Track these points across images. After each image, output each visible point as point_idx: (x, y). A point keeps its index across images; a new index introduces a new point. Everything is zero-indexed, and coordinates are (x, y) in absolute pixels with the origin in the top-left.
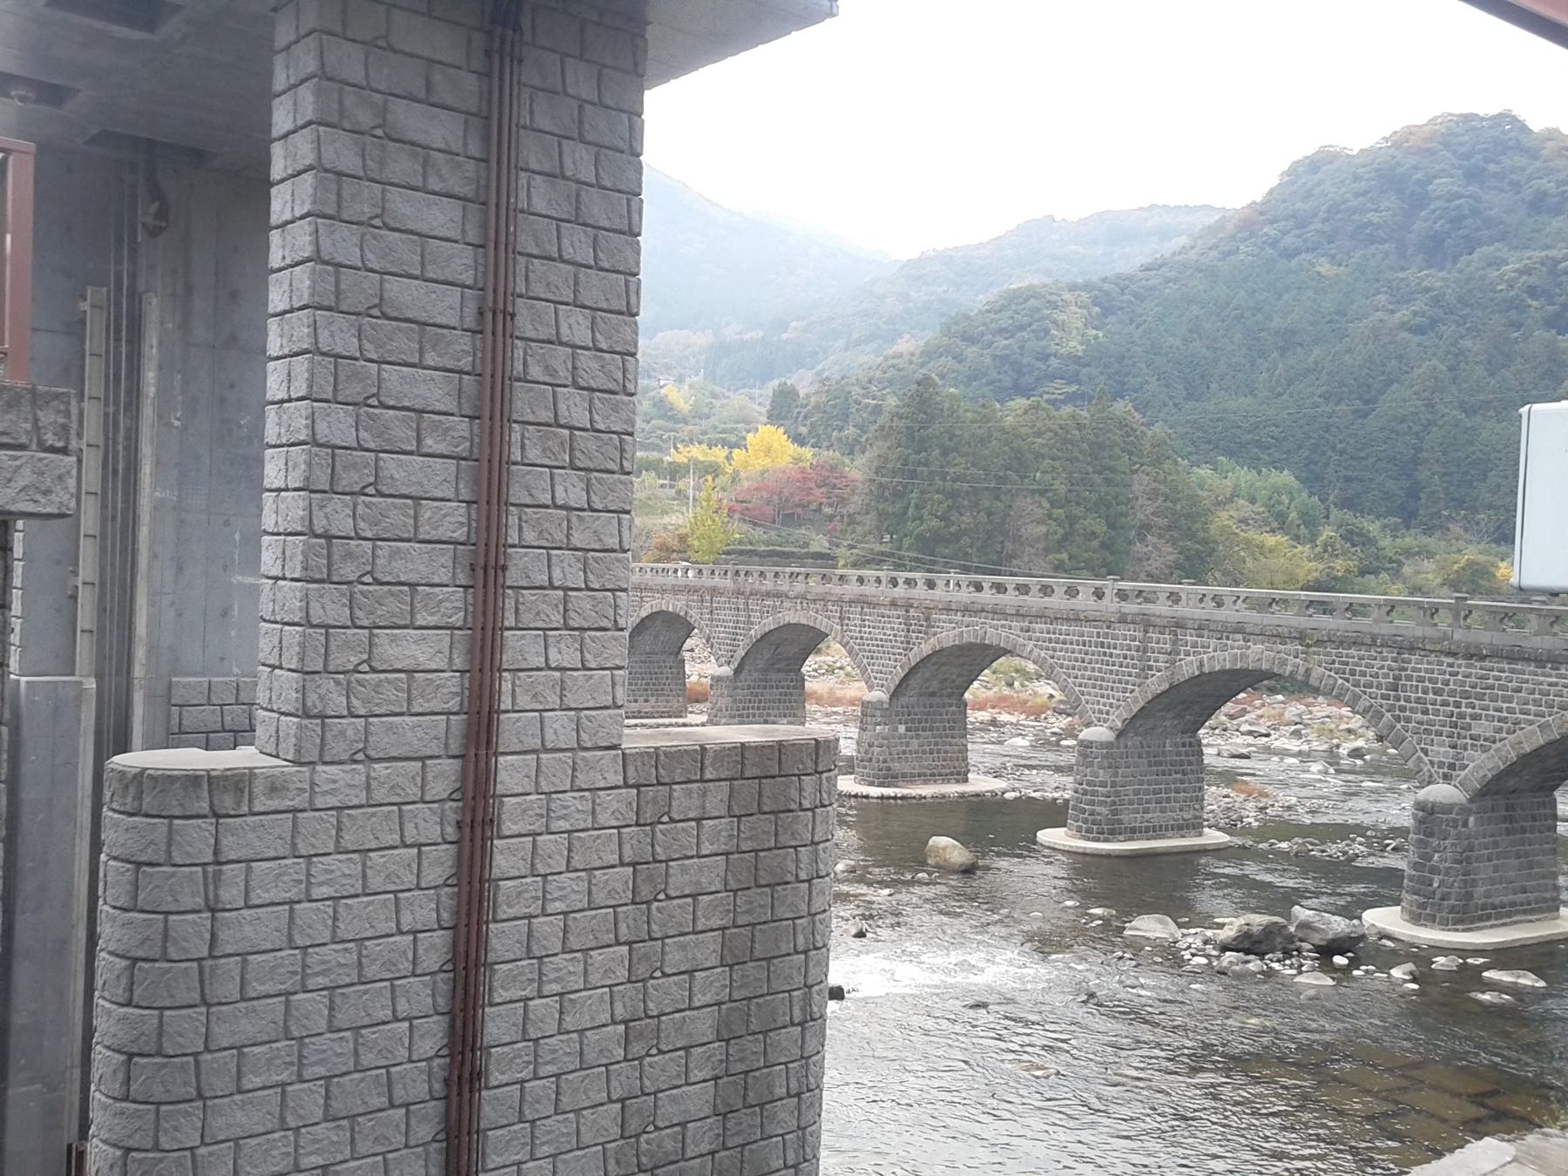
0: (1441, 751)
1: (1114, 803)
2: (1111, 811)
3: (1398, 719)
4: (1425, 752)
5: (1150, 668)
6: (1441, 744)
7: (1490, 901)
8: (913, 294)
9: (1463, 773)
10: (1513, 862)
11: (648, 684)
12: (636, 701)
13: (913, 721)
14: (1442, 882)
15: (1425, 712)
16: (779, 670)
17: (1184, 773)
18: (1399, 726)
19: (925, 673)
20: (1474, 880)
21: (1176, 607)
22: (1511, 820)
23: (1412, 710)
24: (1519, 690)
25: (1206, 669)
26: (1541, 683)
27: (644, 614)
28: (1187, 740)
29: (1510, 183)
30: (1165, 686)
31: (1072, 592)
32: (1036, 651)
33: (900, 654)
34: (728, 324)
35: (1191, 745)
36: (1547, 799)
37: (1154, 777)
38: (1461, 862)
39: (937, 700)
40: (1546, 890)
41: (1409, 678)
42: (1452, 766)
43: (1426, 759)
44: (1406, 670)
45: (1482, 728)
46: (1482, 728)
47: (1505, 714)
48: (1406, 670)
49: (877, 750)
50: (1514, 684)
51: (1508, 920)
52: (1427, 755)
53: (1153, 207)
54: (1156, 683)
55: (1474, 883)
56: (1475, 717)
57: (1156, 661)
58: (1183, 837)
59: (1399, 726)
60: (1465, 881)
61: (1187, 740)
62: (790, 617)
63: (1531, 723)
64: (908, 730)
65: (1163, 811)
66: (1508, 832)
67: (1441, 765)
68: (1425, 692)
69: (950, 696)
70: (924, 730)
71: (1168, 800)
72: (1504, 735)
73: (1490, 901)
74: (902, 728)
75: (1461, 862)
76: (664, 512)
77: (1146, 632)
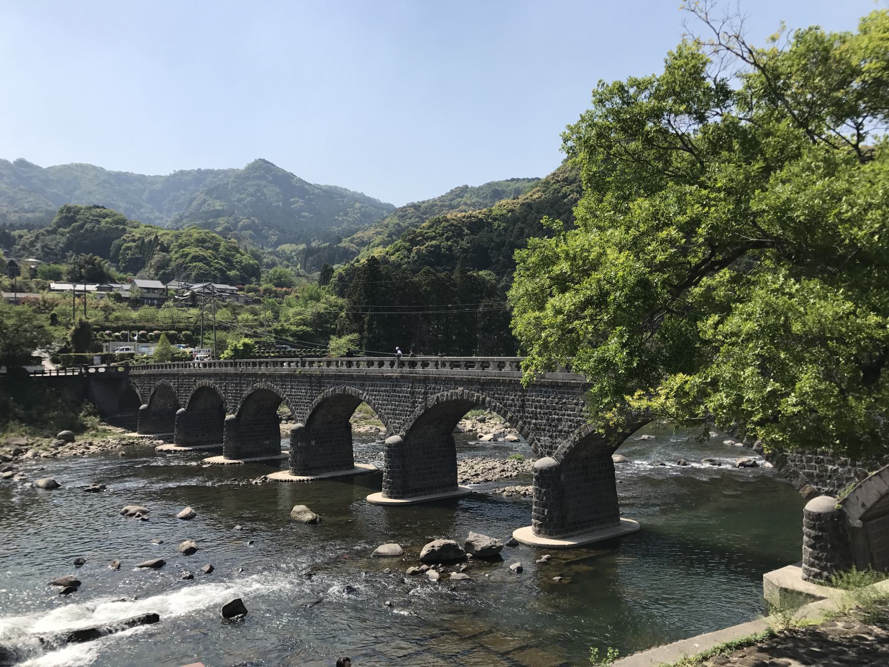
4: (539, 441)
8: (402, 224)
12: (197, 436)
21: (426, 369)
30: (423, 411)
31: (501, 365)
33: (309, 402)
34: (314, 240)
41: (528, 400)
42: (551, 447)
46: (564, 426)
51: (589, 529)
53: (513, 180)
54: (419, 411)
57: (419, 398)
58: (445, 492)
64: (316, 443)
67: (546, 447)
68: (536, 408)
74: (313, 443)
76: (261, 337)
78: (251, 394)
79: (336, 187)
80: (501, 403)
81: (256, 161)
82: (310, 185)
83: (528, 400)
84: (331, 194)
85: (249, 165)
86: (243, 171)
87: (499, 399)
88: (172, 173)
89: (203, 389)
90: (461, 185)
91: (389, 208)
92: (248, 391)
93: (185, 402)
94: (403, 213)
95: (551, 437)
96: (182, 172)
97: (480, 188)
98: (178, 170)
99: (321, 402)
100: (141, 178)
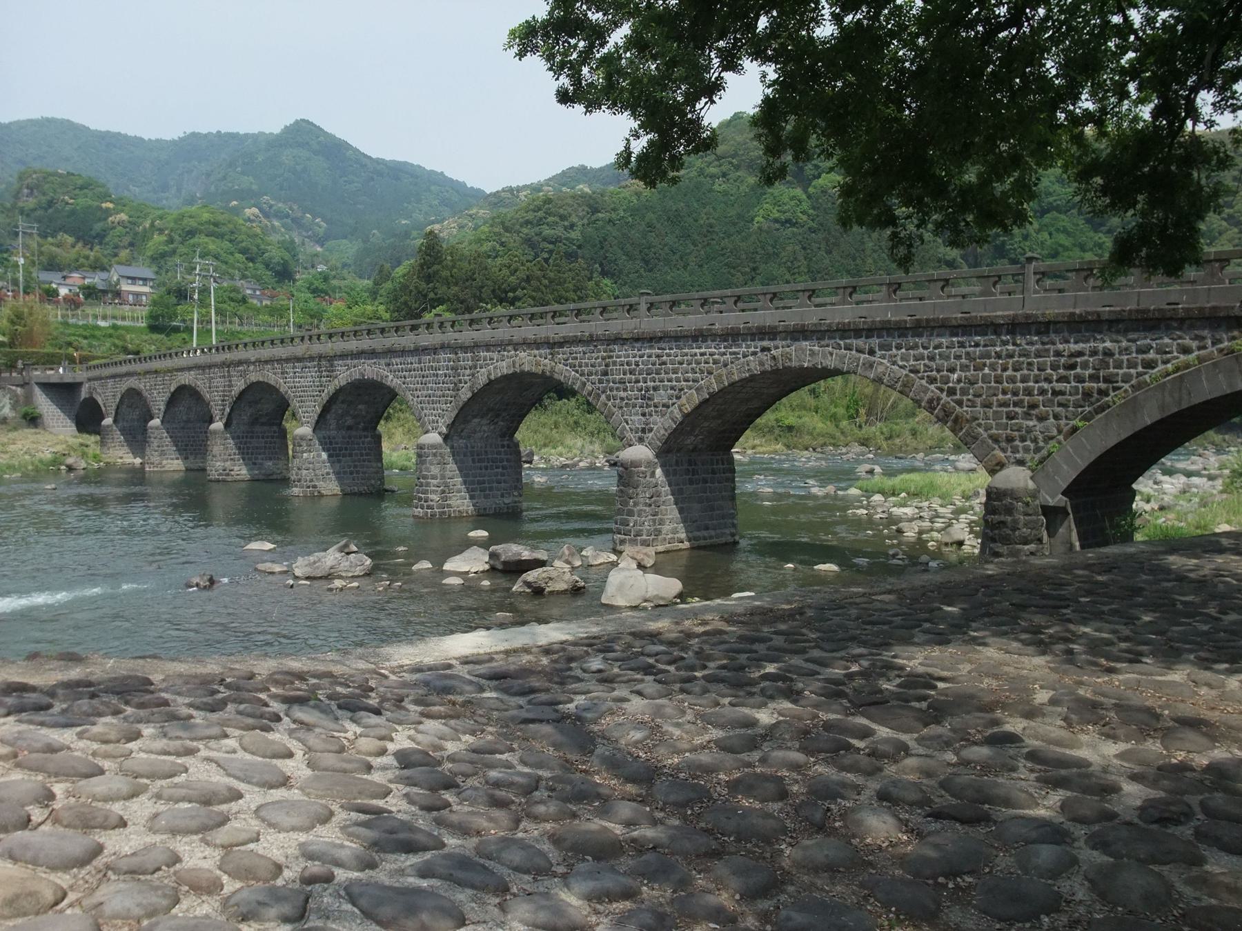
0: (637, 420)
1: (443, 492)
2: (442, 498)
3: (608, 398)
5: (460, 381)
6: (636, 414)
7: (676, 536)
9: (650, 435)
10: (696, 506)
11: (187, 445)
13: (334, 449)
14: (635, 523)
15: (625, 390)
16: (263, 424)
17: (504, 468)
18: (610, 404)
19: (338, 408)
20: (661, 519)
22: (694, 472)
23: (617, 389)
24: (681, 363)
25: (492, 377)
26: (696, 355)
27: (172, 390)
28: (505, 443)
29: (995, 370)
32: (395, 380)
35: (509, 446)
36: (725, 457)
37: (479, 471)
38: (650, 505)
39: (354, 433)
40: (726, 527)
41: (614, 363)
42: (643, 431)
43: (627, 427)
44: (612, 357)
45: (661, 397)
46: (661, 397)
47: (674, 383)
48: (612, 357)
49: (305, 472)
50: (679, 358)
52: (627, 424)
54: (465, 395)
55: (662, 522)
56: (655, 389)
59: (610, 404)
60: (654, 521)
61: (505, 443)
62: (254, 377)
63: (690, 388)
65: (486, 497)
66: (691, 482)
69: (365, 429)
70: (344, 456)
71: (491, 489)
72: (674, 400)
73: (676, 536)
75: (650, 505)
77: (456, 354)
78: (244, 390)
79: (405, 163)
80: (577, 372)
81: (297, 122)
82: (370, 158)
83: (614, 363)
84: (398, 172)
85: (286, 127)
86: (277, 135)
87: (575, 366)
88: (182, 135)
89: (182, 389)
90: (576, 165)
91: (477, 194)
92: (239, 385)
93: (159, 410)
94: (497, 200)
95: (644, 415)
96: (194, 134)
97: (601, 169)
98: (188, 132)
99: (334, 394)
100: (138, 141)
